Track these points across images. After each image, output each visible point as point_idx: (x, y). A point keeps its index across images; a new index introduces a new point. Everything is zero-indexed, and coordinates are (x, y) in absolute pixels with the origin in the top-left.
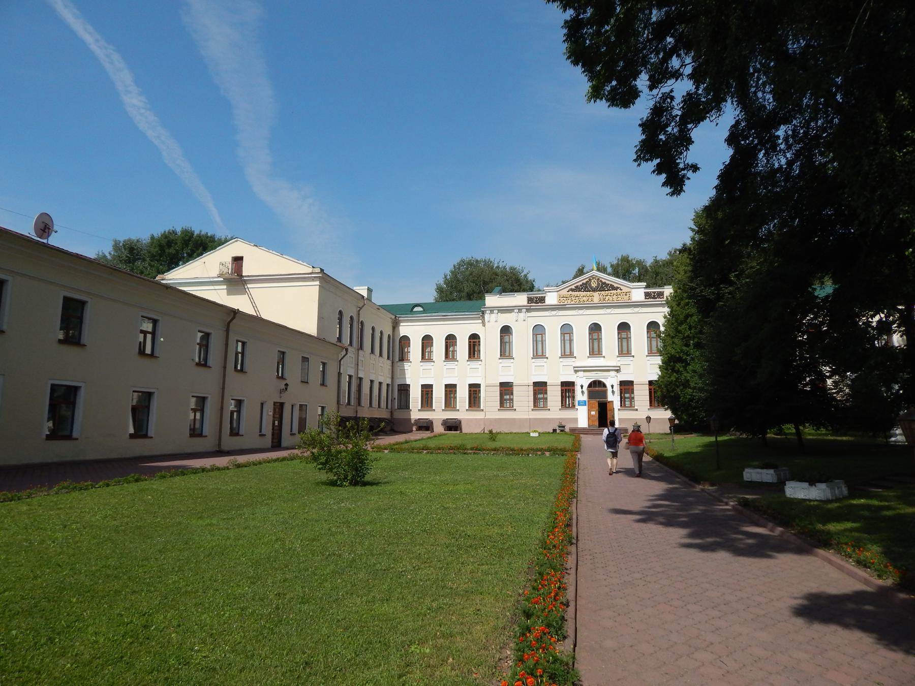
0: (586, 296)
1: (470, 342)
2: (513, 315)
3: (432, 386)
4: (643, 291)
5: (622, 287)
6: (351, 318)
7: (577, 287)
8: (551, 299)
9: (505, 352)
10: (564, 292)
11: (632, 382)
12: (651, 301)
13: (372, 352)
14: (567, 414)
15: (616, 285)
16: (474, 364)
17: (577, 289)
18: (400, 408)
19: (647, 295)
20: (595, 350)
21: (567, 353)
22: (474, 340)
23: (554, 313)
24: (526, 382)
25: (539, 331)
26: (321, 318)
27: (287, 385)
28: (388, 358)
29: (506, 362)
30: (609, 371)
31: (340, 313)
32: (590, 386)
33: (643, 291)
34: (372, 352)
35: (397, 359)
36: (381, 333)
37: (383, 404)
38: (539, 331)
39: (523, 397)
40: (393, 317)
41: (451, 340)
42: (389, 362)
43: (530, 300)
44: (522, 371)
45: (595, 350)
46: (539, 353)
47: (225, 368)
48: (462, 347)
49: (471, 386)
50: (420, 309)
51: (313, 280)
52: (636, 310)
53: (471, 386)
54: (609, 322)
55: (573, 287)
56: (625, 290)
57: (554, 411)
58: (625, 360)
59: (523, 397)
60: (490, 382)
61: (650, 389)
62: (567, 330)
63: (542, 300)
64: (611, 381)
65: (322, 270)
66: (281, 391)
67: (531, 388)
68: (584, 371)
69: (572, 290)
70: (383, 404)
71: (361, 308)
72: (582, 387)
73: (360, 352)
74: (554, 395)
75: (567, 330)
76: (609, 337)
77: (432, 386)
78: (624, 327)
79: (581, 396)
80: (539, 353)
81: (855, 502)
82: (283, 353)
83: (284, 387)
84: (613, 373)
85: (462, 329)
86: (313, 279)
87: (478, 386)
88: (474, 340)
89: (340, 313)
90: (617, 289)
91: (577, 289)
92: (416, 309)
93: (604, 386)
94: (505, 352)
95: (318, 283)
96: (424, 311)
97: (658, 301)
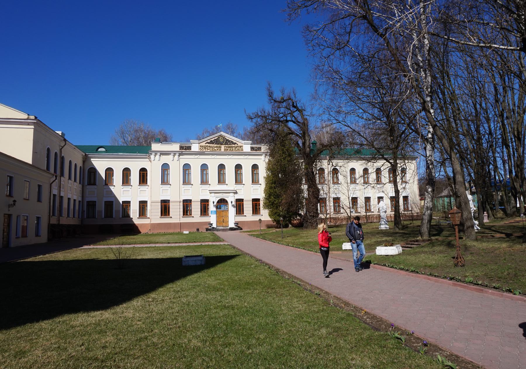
0: (217, 147)
1: (140, 173)
2: (171, 157)
3: (130, 202)
4: (250, 146)
5: (238, 143)
6: (56, 153)
7: (211, 141)
8: (195, 147)
9: (165, 181)
10: (203, 144)
11: (243, 200)
12: (254, 152)
13: (70, 178)
14: (204, 219)
15: (234, 142)
16: (143, 188)
17: (211, 142)
18: (88, 217)
19: (252, 149)
20: (221, 180)
21: (204, 181)
22: (143, 173)
23: (197, 156)
24: (178, 200)
25: (187, 168)
26: (35, 153)
27: (15, 201)
28: (80, 183)
29: (166, 187)
30: (229, 193)
31: (48, 150)
32: (218, 202)
33: (250, 146)
34: (70, 178)
35: (86, 183)
36: (76, 165)
37: (76, 215)
38: (187, 168)
39: (176, 210)
40: (84, 154)
41: (126, 172)
42: (81, 186)
43: (181, 148)
44: (176, 193)
45: (221, 180)
46: (186, 181)
47: (60, 187)
48: (135, 177)
49: (141, 202)
50: (103, 150)
51: (28, 125)
52: (246, 157)
53: (141, 202)
54: (247, 164)
55: (209, 141)
56: (239, 144)
57: (196, 217)
58: (238, 187)
59: (176, 210)
60: (154, 199)
61: (253, 204)
62: (204, 168)
63: (189, 148)
64: (231, 199)
65: (36, 118)
66: (10, 206)
67: (182, 203)
68: (215, 193)
69: (208, 143)
70: (76, 215)
71: (63, 147)
72: (214, 202)
73: (62, 178)
74: (196, 208)
75: (204, 168)
76: (230, 173)
77: (130, 202)
78: (238, 167)
79: (212, 208)
80: (186, 181)
81: (60, 256)
82: (11, 178)
83: (12, 203)
84: (232, 194)
85: (135, 165)
86: (28, 124)
87: (146, 202)
88: (143, 173)
89: (48, 150)
90: (235, 143)
91: (211, 142)
92: (100, 150)
93: (227, 202)
94: (165, 181)
95: (33, 127)
96: (107, 151)
97: (258, 152)
